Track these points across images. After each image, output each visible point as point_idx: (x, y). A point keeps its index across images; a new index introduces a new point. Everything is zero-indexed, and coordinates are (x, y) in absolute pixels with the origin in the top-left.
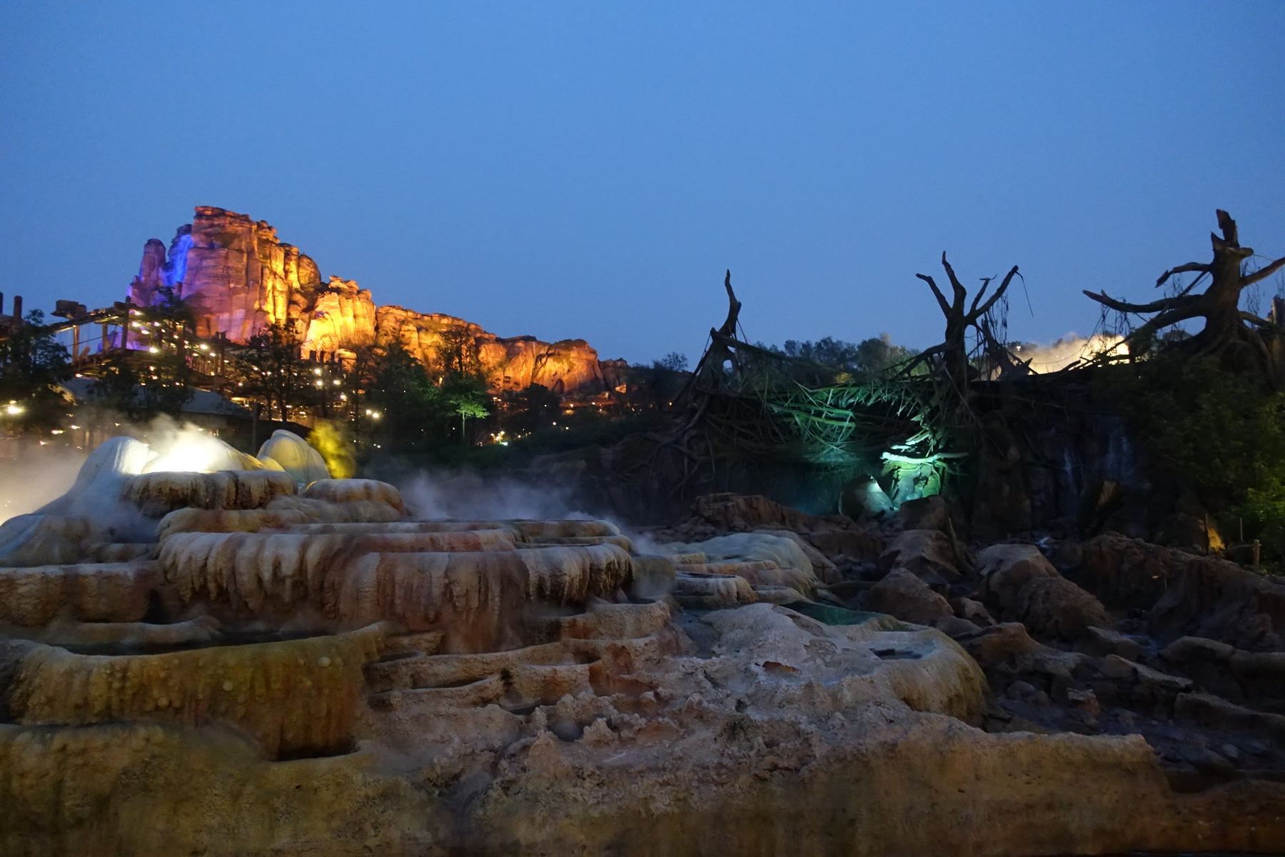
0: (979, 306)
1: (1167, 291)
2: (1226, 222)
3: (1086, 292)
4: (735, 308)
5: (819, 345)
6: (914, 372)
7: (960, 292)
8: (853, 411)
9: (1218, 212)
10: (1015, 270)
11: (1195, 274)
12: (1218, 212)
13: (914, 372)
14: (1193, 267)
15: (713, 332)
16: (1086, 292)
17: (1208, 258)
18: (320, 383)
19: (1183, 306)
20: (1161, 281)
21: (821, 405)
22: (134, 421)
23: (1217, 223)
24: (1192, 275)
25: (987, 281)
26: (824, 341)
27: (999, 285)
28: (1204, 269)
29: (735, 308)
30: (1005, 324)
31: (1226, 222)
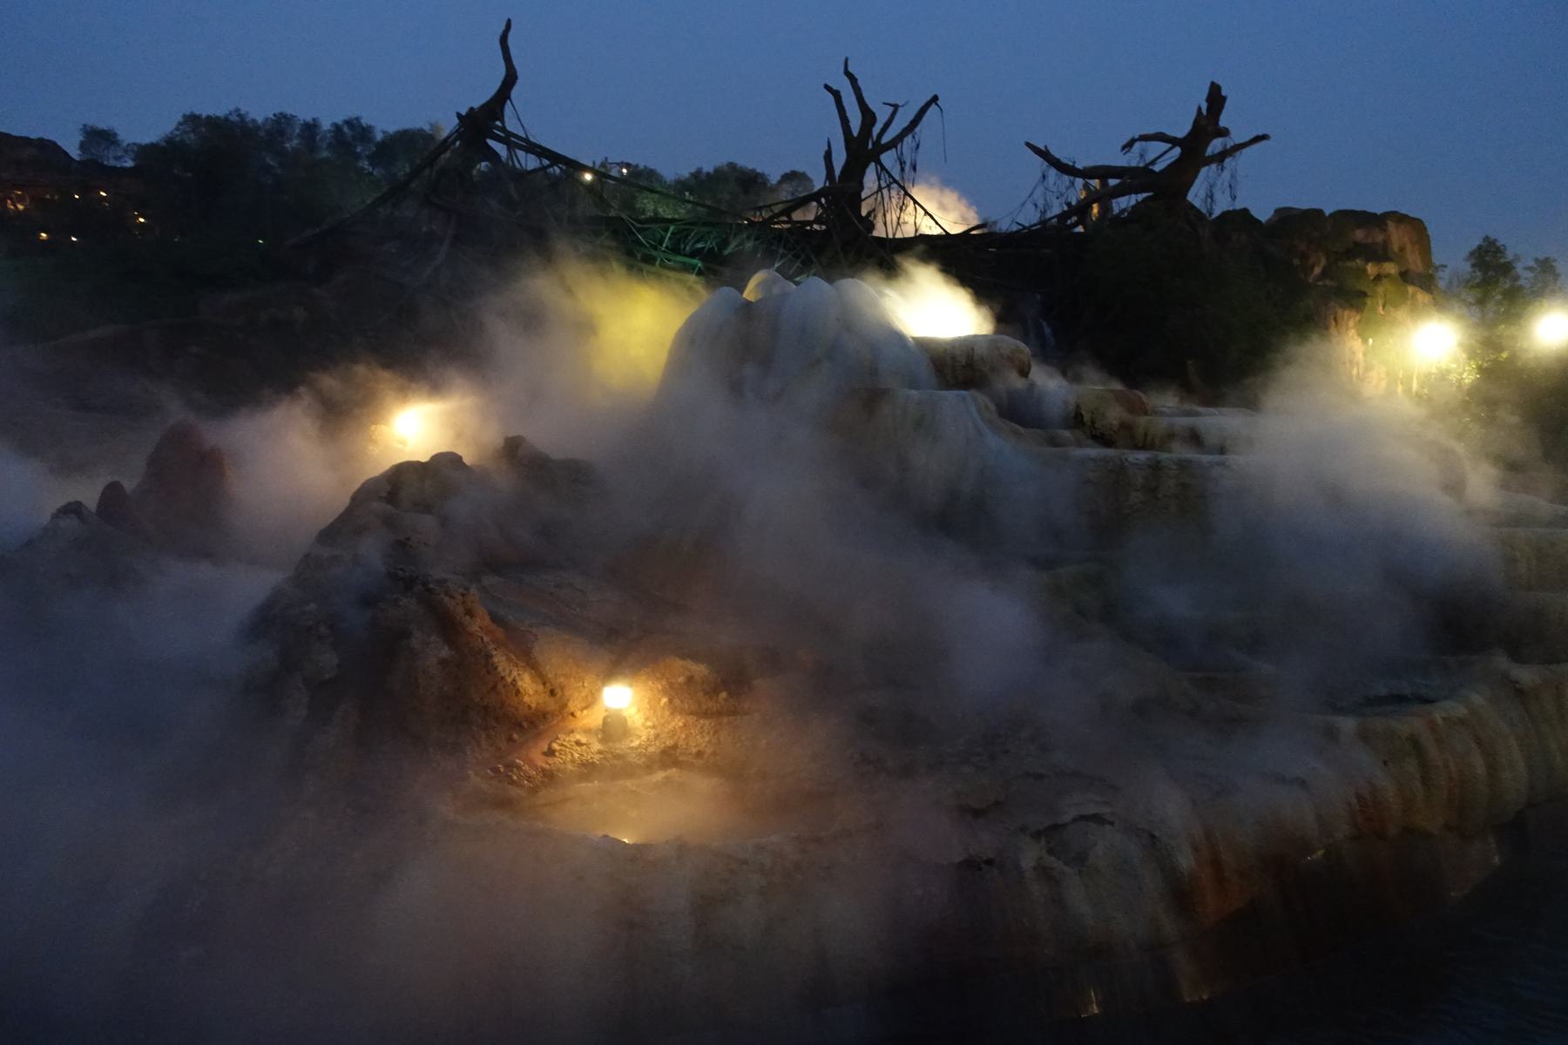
0: (885, 139)
1: (1131, 160)
2: (1216, 99)
3: (1028, 144)
4: (510, 79)
5: (337, 128)
6: (797, 216)
7: (868, 116)
8: (703, 260)
9: (1213, 84)
10: (935, 99)
11: (1165, 146)
12: (1213, 84)
13: (797, 216)
14: (1160, 137)
15: (459, 115)
16: (1028, 144)
17: (1182, 130)
18: (1080, 229)
19: (1134, 178)
20: (1129, 145)
21: (655, 248)
22: (630, 268)
23: (1205, 95)
24: (1158, 147)
25: (896, 107)
26: (348, 123)
27: (911, 117)
28: (1174, 142)
29: (510, 79)
30: (914, 169)
31: (1216, 99)
